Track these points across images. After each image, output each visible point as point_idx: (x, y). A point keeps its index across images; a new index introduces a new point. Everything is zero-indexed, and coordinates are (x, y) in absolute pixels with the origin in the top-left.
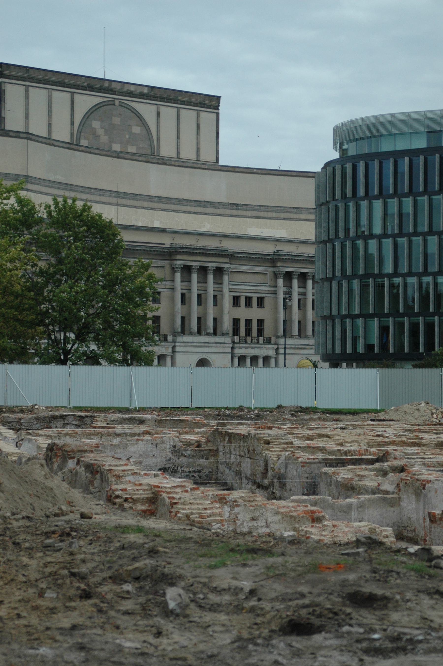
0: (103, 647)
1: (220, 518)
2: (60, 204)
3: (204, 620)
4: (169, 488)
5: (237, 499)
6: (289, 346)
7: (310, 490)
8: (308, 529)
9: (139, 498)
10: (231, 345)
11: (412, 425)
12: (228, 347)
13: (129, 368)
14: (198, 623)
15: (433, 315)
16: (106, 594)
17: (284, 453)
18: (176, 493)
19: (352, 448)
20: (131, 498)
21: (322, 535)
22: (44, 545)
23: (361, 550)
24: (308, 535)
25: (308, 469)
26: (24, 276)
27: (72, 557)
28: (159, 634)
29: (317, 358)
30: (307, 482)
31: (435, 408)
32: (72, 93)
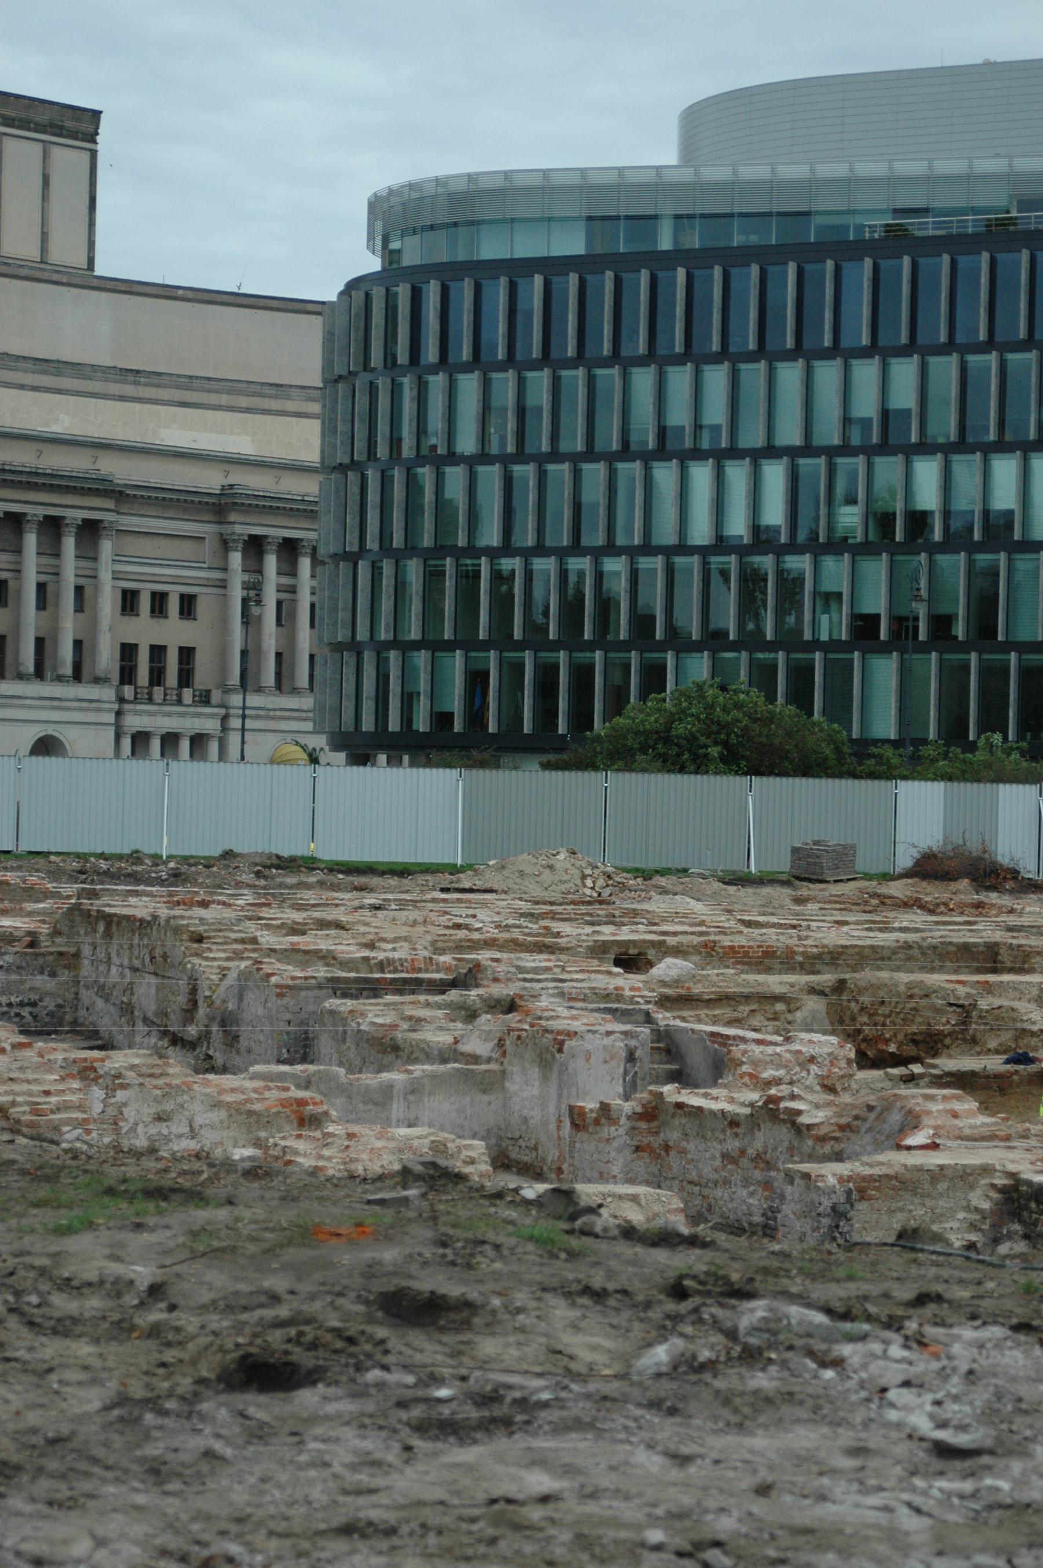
1: (80, 1116)
3: (38, 1355)
5: (123, 1071)
7: (296, 1052)
10: (116, 706)
11: (537, 903)
14: (25, 1363)
15: (591, 646)
17: (236, 963)
19: (396, 955)
21: (320, 1157)
23: (412, 1192)
24: (288, 1158)
29: (319, 742)
30: (288, 1033)
31: (590, 864)
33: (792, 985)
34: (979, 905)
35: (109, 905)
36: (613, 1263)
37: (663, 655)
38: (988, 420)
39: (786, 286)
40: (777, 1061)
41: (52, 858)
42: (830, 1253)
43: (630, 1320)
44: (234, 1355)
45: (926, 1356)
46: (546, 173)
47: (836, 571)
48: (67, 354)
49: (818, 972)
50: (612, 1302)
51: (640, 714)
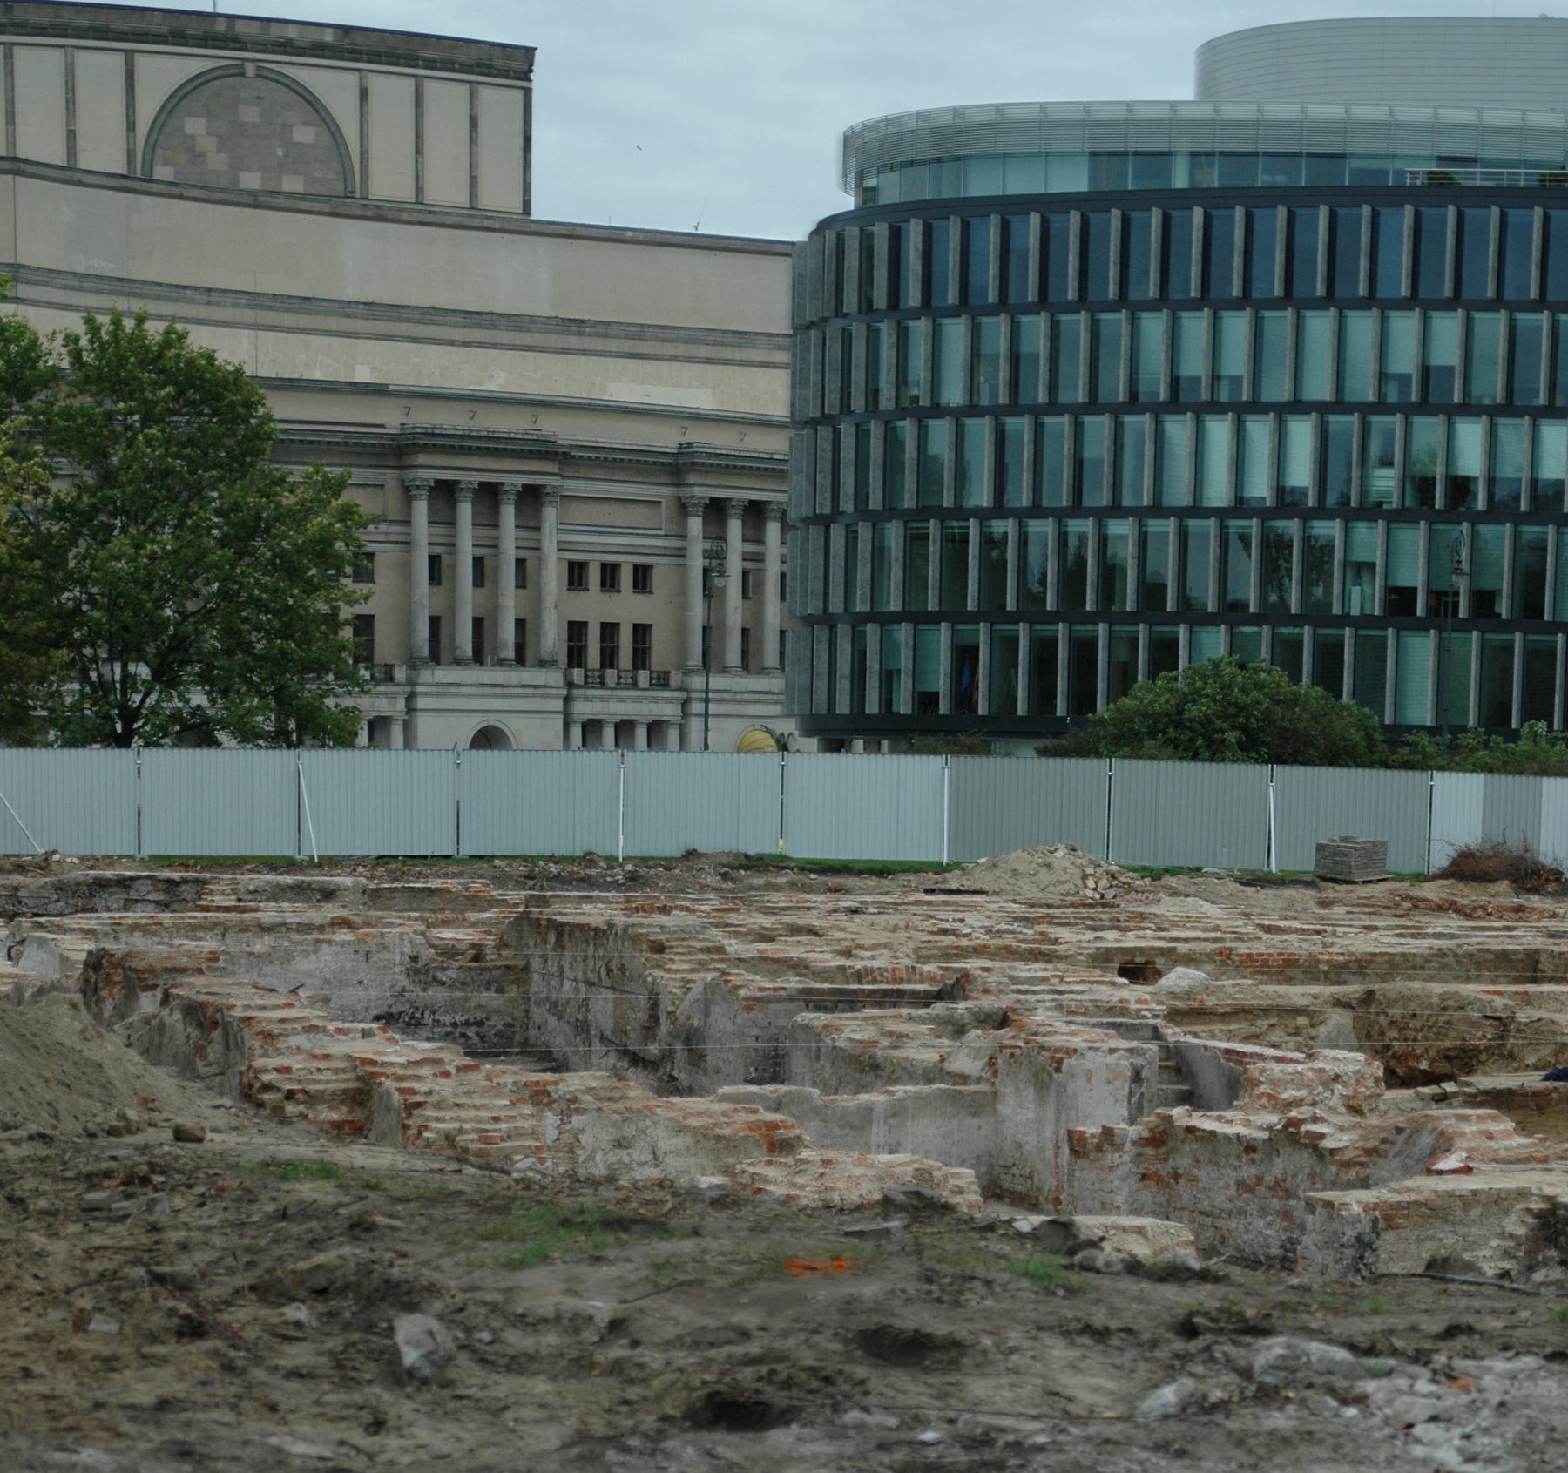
0: (238, 1452)
1: (533, 1143)
2: (103, 331)
3: (492, 1393)
4: (402, 1066)
5: (580, 1096)
6: (718, 696)
7: (765, 1071)
8: (757, 1170)
9: (323, 1092)
10: (565, 692)
11: (1032, 906)
12: (557, 697)
13: (292, 753)
14: (478, 1400)
15: (1093, 618)
16: (243, 1327)
17: (702, 975)
18: (419, 1078)
19: (875, 964)
20: (304, 1092)
21: (793, 1185)
22: (84, 1205)
23: (895, 1224)
24: (757, 1185)
25: (760, 1016)
26: (17, 519)
27: (155, 1237)
28: (377, 1425)
29: (789, 726)
30: (756, 1050)
31: (1092, 862)
32: (129, 53)
33: (1315, 997)
34: (1519, 909)
35: (560, 914)
36: (1116, 1300)
37: (1174, 629)
38: (1538, 382)
39: (1316, 231)
40: (1298, 1081)
41: (497, 862)
42: (1353, 1286)
43: (1135, 1360)
44: (700, 1393)
45: (1455, 1390)
46: (1043, 107)
47: (1369, 539)
48: (502, 303)
49: (1345, 983)
50: (1115, 1341)
51: (1148, 694)
